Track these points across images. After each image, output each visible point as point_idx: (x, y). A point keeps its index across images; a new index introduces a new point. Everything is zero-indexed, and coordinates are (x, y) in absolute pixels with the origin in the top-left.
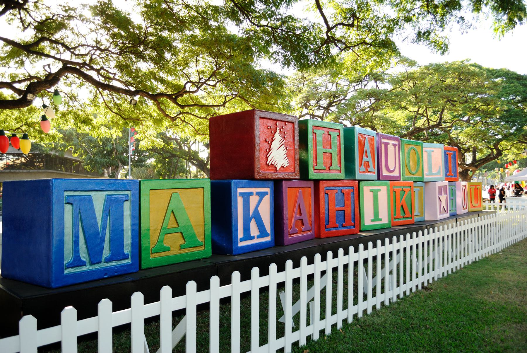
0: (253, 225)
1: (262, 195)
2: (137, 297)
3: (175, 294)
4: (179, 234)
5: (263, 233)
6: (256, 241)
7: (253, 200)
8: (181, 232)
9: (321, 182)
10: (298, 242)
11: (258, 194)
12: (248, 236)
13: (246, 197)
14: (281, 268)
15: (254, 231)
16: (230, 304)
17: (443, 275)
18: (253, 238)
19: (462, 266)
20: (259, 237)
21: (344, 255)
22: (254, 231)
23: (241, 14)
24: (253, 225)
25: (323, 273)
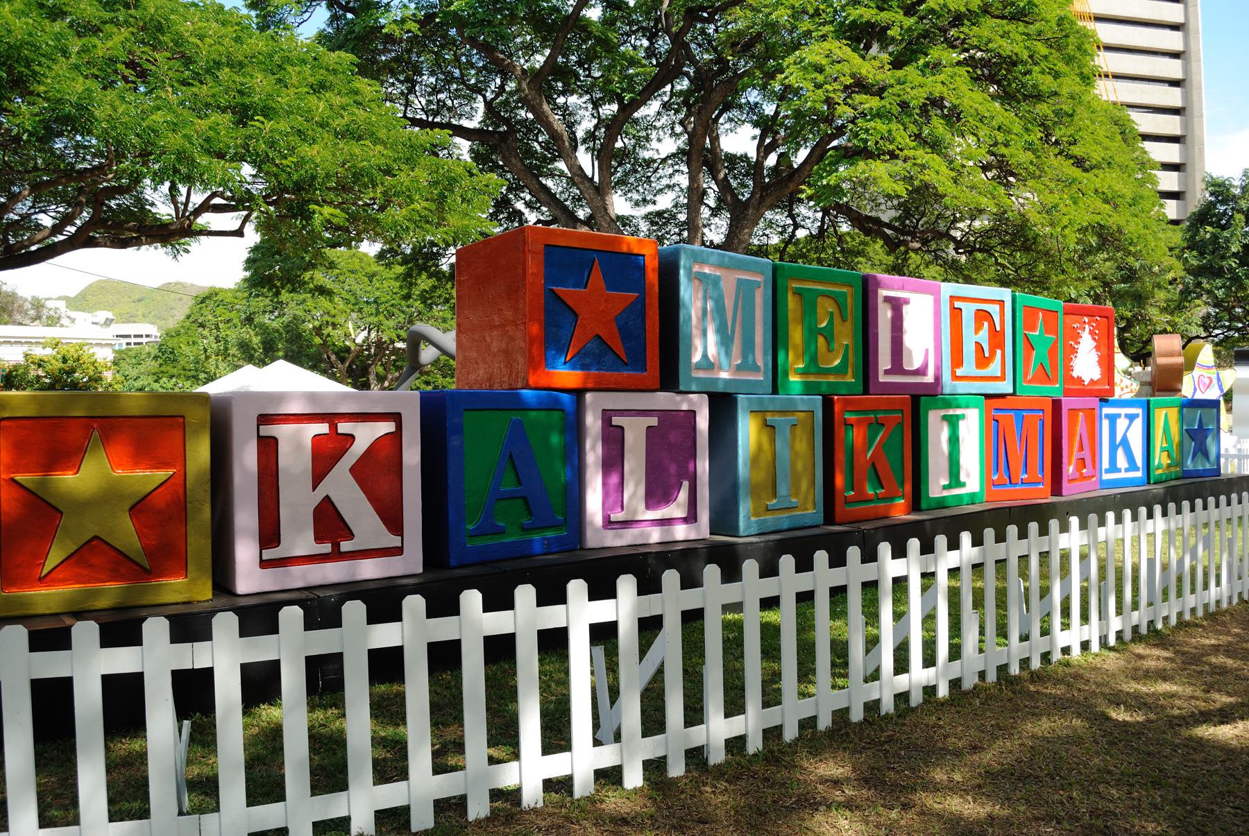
0: (1120, 453)
1: (1131, 418)
2: (525, 594)
3: (542, 601)
4: (519, 502)
5: (1132, 466)
6: (1123, 475)
7: (1122, 424)
8: (525, 498)
9: (261, 434)
10: (772, 529)
11: (1127, 416)
12: (1113, 468)
13: (1113, 419)
14: (838, 560)
15: (1122, 462)
16: (703, 618)
17: (1230, 602)
18: (1119, 471)
19: (1173, 621)
20: (1127, 470)
21: (1040, 535)
22: (1122, 462)
23: (850, 145)
24: (1120, 453)
25: (977, 567)
